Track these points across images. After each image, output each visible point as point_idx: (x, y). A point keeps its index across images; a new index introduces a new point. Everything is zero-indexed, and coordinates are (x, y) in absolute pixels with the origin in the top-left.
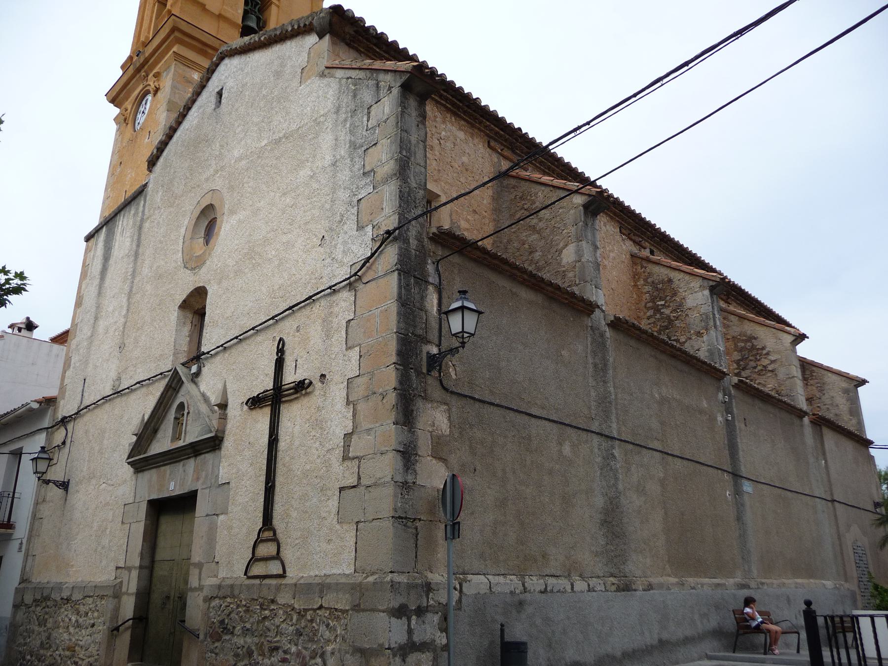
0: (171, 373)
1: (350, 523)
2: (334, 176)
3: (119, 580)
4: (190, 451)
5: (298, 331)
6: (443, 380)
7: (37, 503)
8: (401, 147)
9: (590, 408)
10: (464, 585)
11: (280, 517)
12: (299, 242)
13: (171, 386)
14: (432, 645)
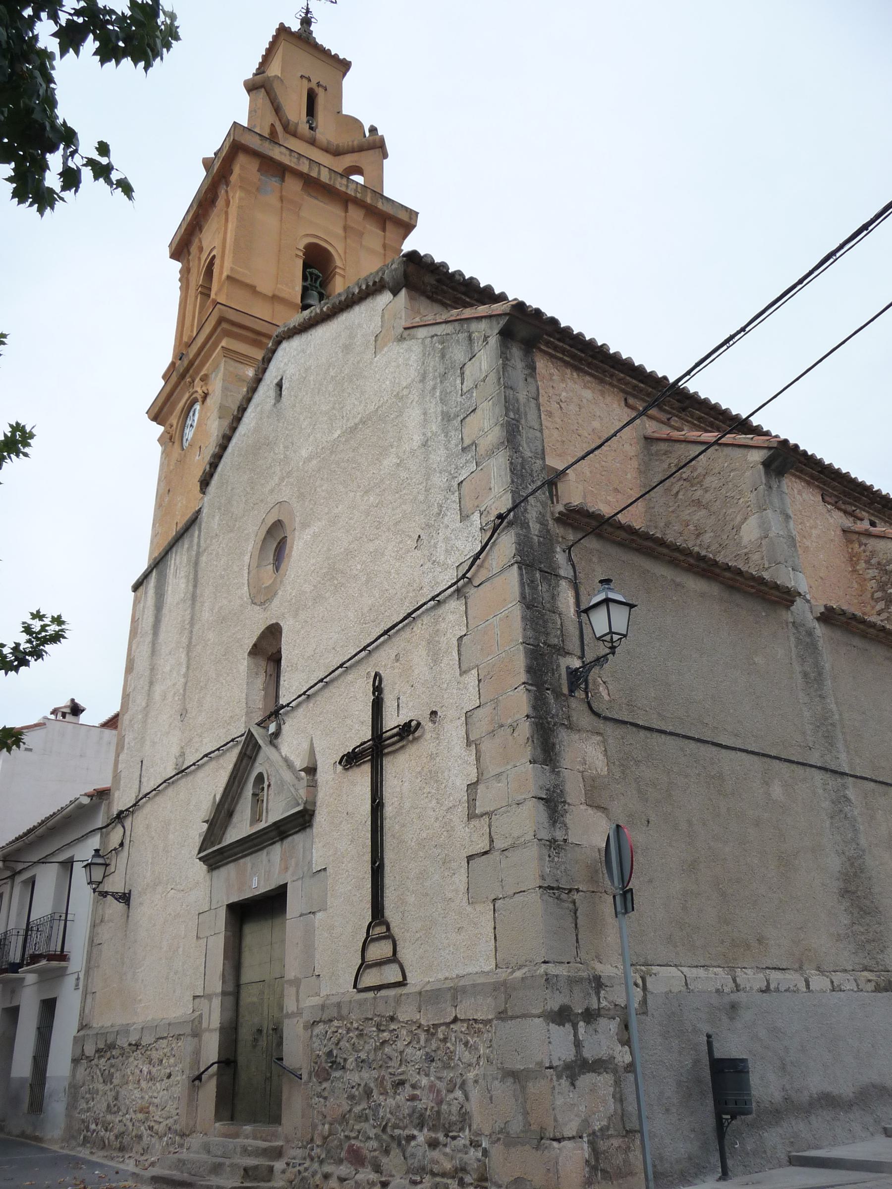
0: (243, 738)
1: (484, 902)
2: (426, 459)
3: (197, 1014)
4: (274, 833)
5: (397, 660)
6: (592, 702)
7: (94, 926)
8: (507, 409)
9: (804, 733)
10: (649, 980)
11: (392, 905)
12: (390, 548)
13: (245, 754)
14: (611, 1063)
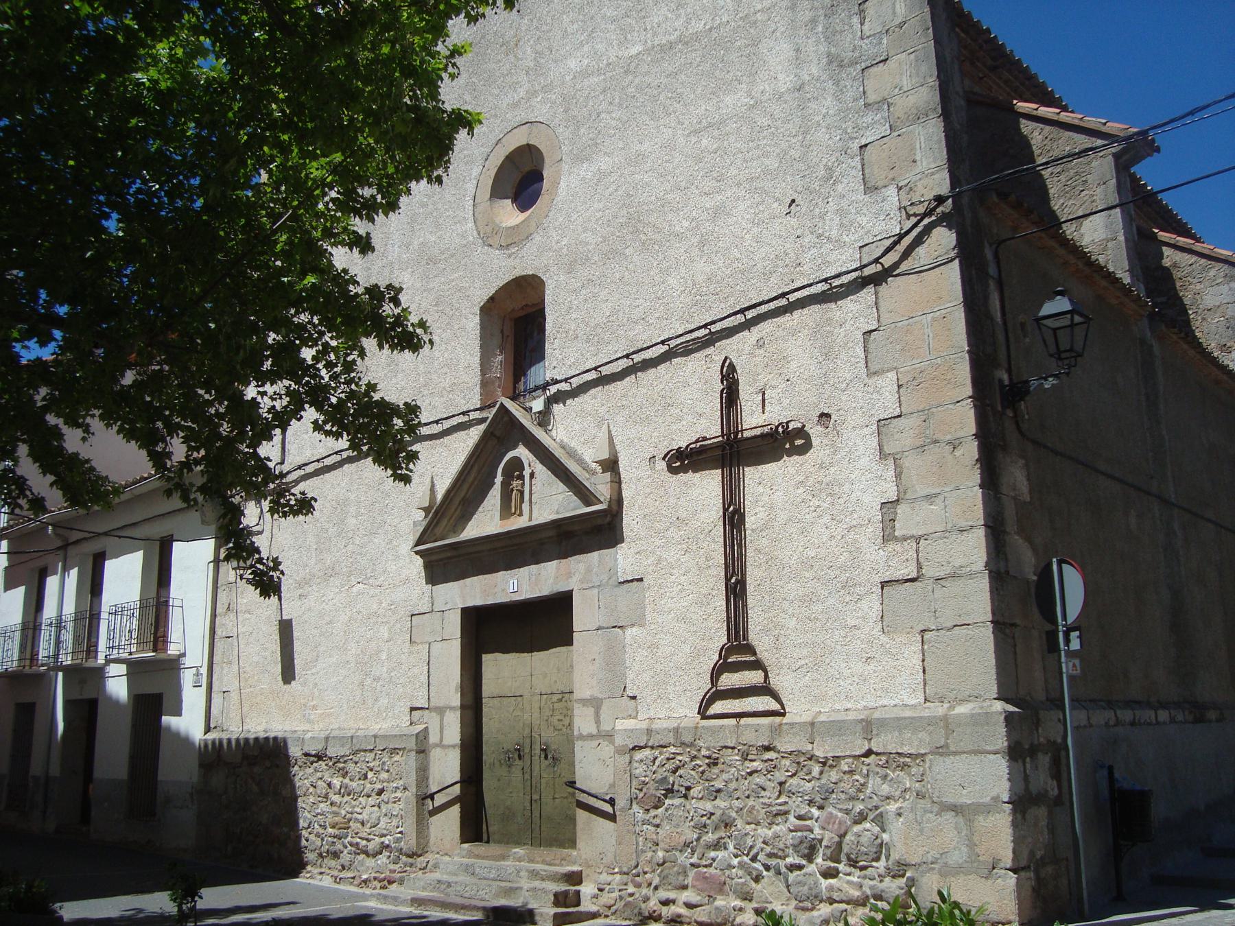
11: (758, 628)
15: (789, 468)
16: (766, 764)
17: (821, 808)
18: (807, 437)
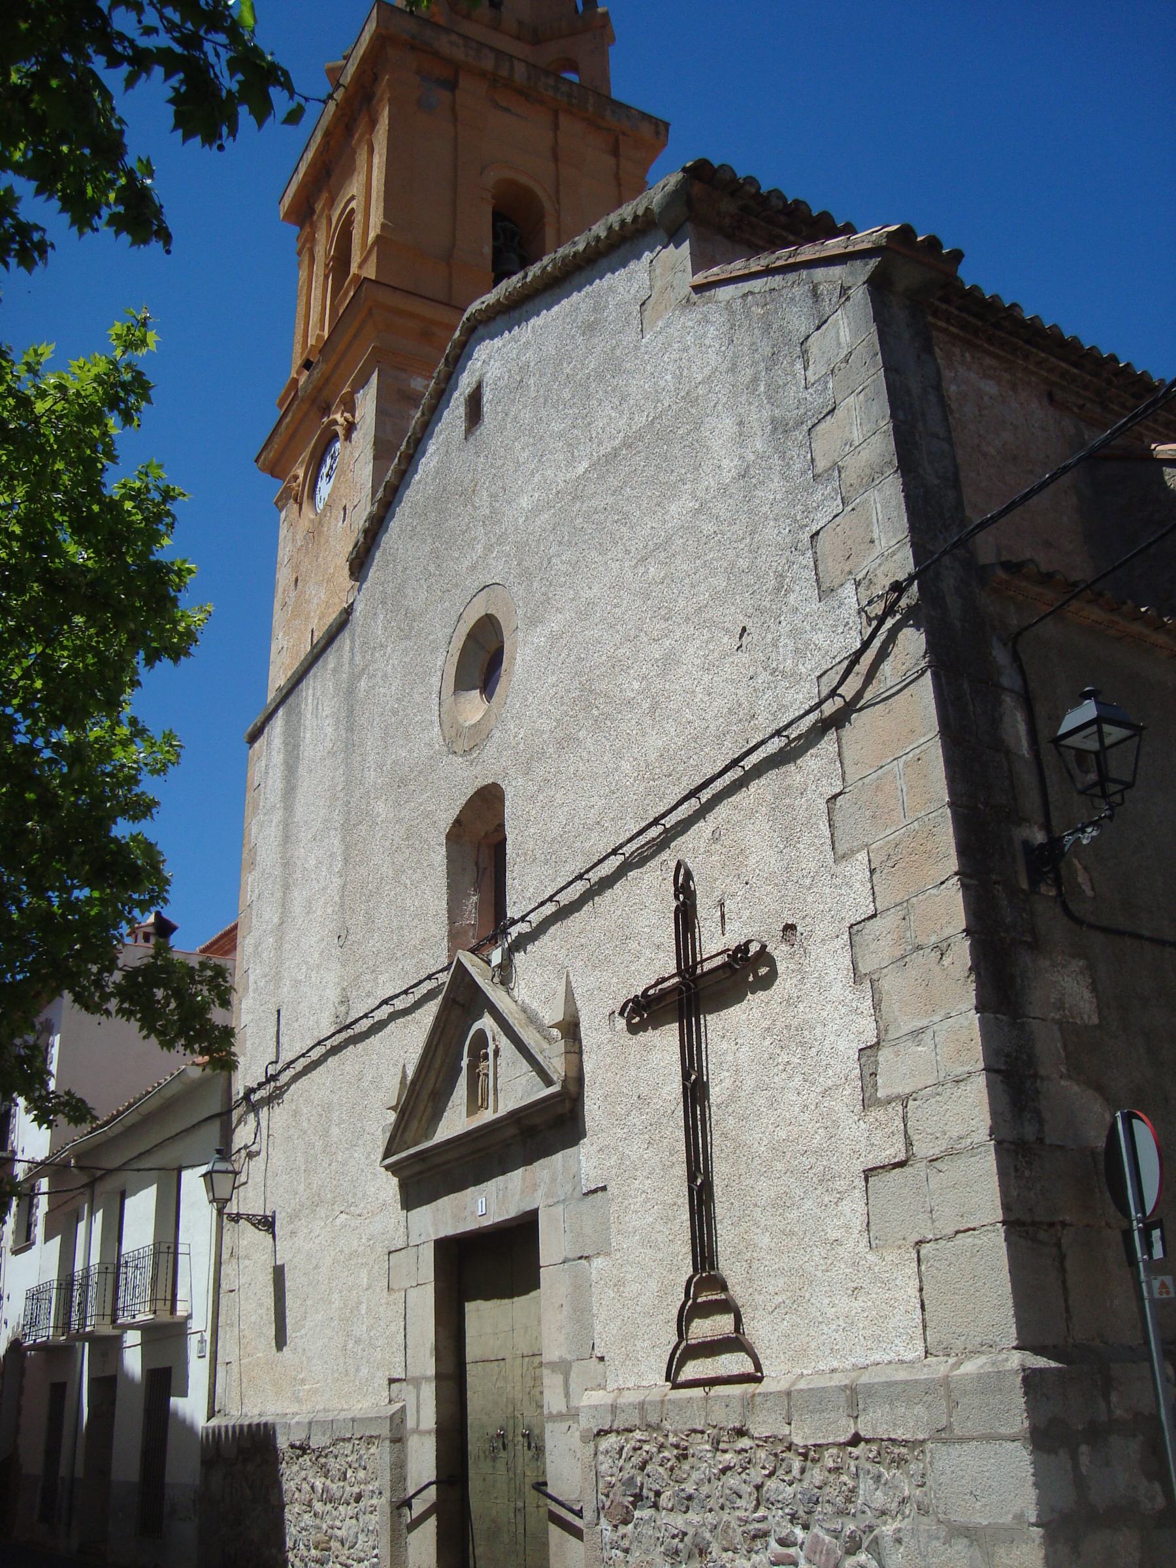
3: (397, 1406)
11: (730, 1250)
12: (691, 650)
15: (754, 1010)
16: (740, 1457)
17: (806, 1527)
18: (771, 962)
